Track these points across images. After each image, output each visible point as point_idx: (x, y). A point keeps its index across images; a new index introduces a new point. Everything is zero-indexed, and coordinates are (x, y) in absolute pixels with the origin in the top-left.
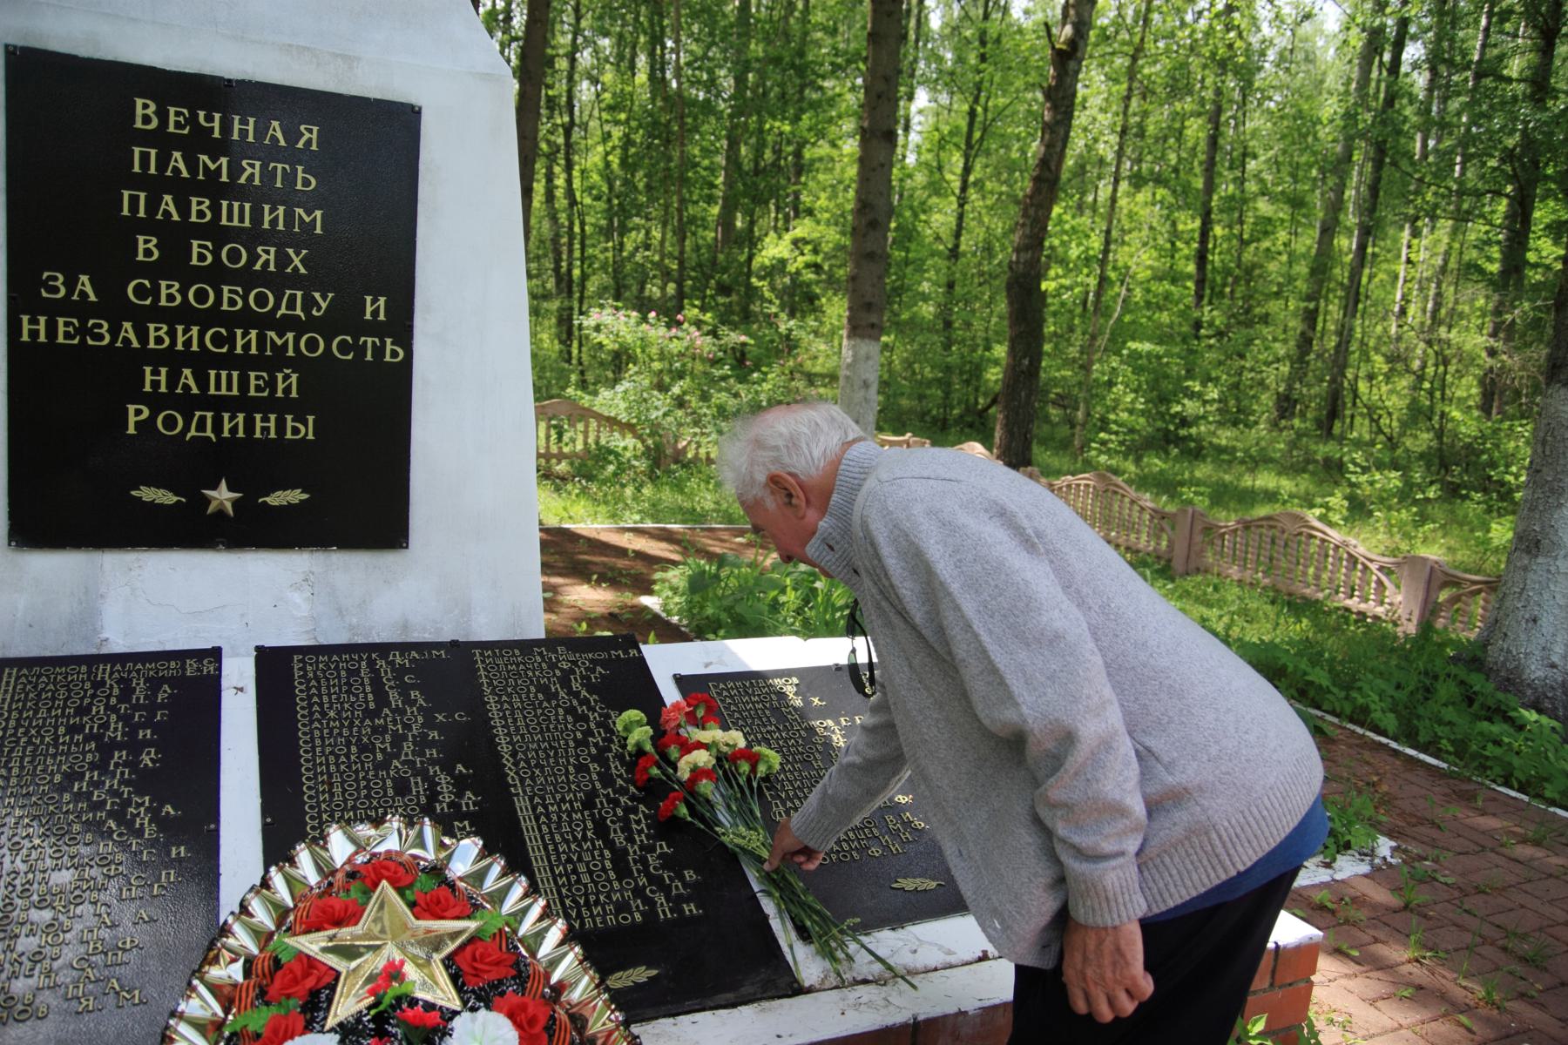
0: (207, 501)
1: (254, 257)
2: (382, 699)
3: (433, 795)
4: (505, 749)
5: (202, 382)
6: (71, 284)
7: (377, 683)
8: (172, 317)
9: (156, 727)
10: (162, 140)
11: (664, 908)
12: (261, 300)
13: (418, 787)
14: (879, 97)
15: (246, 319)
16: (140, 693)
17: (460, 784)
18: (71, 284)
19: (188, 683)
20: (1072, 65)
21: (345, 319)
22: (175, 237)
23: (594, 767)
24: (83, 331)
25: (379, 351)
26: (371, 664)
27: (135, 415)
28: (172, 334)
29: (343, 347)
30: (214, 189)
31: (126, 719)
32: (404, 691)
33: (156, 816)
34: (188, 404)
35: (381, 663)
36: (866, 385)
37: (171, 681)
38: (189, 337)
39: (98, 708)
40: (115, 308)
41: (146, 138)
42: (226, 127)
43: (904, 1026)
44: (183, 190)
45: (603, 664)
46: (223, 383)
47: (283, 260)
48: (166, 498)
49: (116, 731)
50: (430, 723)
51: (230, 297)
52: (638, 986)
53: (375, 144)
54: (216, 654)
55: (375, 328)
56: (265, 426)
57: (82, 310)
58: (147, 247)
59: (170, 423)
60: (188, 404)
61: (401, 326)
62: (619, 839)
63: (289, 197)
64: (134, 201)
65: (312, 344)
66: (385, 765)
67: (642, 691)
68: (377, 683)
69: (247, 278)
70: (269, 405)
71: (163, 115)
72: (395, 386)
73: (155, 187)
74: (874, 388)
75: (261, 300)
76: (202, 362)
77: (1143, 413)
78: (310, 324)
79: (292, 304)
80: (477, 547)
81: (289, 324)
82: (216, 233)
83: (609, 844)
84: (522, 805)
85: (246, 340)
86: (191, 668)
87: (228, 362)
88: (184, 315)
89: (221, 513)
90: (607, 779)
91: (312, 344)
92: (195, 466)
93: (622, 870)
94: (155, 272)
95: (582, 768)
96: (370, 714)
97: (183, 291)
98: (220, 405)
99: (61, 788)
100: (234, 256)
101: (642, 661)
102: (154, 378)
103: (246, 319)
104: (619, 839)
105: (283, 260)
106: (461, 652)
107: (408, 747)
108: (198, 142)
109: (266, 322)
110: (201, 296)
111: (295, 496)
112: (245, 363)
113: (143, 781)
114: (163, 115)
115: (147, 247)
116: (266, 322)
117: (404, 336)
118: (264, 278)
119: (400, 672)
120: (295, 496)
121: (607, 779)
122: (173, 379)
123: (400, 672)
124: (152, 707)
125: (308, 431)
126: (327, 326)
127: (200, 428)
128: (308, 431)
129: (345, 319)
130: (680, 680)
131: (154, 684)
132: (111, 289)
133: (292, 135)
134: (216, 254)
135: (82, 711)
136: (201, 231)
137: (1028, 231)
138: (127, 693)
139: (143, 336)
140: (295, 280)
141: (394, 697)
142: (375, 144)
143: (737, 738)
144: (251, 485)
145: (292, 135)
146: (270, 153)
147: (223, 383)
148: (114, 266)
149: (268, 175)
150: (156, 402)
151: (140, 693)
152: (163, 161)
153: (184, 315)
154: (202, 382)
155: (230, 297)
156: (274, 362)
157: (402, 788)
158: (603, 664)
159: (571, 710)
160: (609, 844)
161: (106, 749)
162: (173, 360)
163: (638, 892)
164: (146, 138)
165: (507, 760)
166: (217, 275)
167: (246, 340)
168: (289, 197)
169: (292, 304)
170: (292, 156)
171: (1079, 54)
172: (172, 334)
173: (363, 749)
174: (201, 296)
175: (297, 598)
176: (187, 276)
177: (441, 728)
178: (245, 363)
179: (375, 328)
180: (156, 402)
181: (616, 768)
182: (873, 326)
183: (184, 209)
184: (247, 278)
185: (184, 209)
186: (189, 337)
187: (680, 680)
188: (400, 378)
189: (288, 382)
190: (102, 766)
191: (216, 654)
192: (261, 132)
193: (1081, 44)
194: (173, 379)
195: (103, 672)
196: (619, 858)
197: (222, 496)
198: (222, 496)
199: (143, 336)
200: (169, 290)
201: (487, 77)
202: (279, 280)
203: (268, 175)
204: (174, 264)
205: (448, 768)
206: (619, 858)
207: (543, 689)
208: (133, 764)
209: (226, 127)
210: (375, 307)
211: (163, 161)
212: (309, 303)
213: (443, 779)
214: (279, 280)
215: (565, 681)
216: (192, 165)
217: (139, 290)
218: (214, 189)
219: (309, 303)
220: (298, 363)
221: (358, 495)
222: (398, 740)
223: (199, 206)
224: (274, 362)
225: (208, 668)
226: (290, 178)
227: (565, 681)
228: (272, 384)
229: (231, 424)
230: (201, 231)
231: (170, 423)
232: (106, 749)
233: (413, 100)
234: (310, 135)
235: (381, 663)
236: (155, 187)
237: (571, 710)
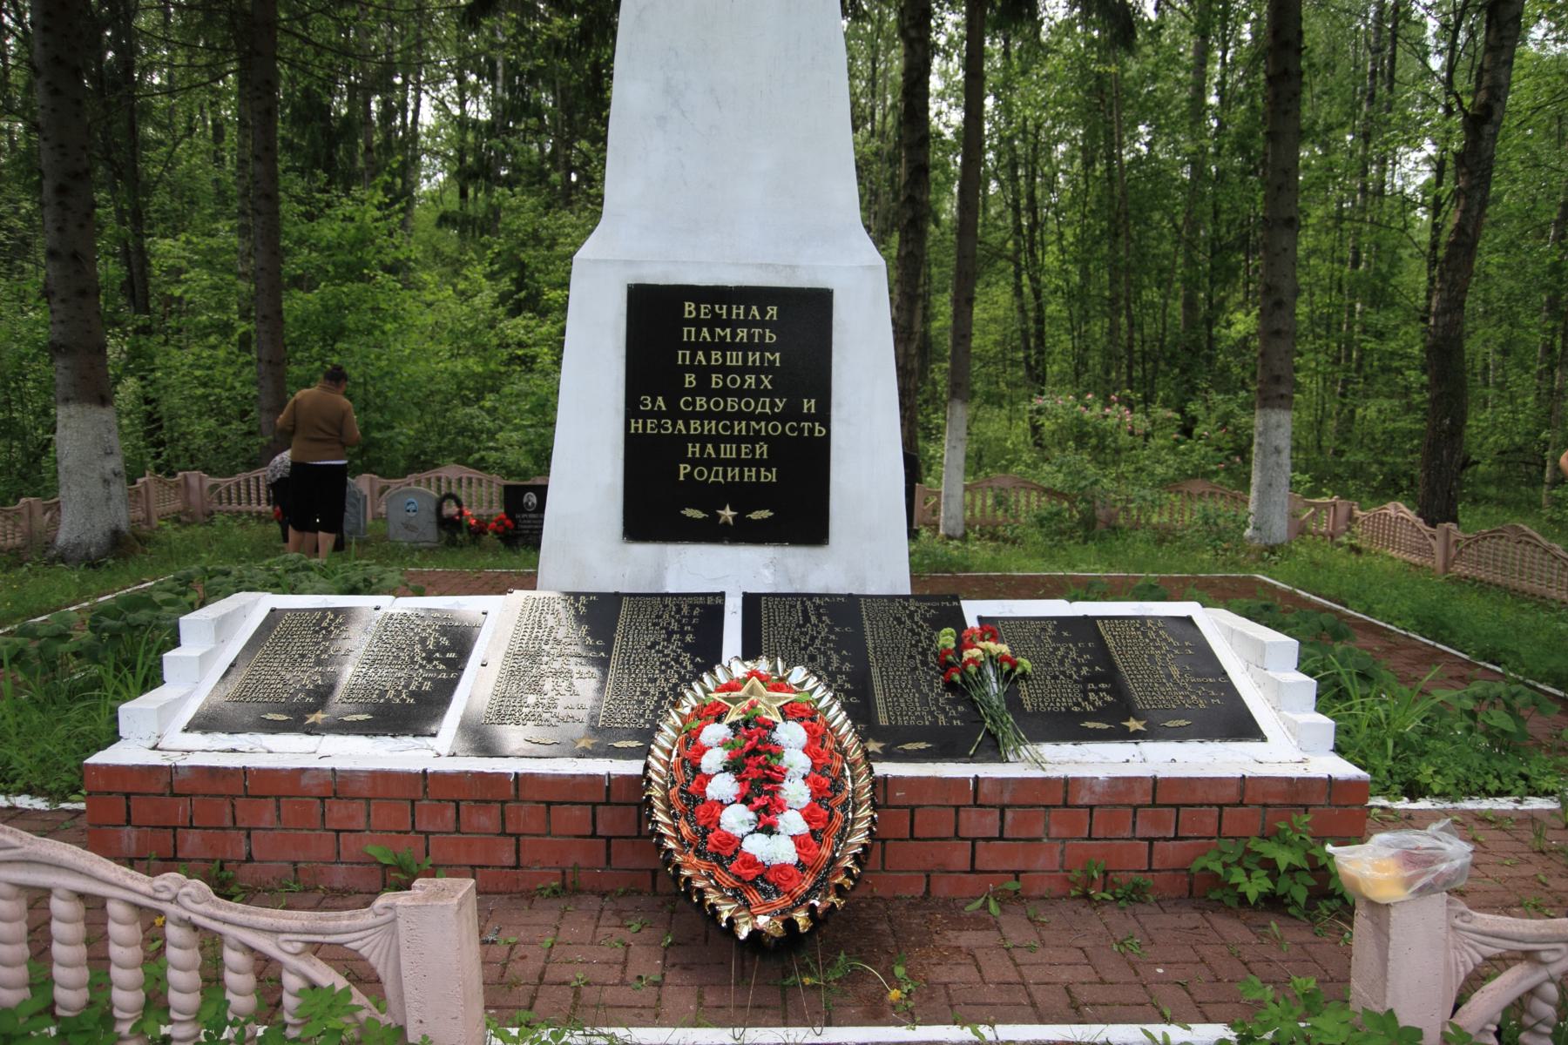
0: (719, 516)
1: (744, 381)
2: (807, 619)
3: (829, 663)
4: (870, 644)
5: (717, 451)
6: (654, 402)
7: (805, 611)
8: (701, 416)
9: (693, 626)
10: (697, 323)
11: (942, 720)
12: (748, 405)
13: (821, 659)
14: (1279, 188)
15: (740, 416)
16: (685, 611)
17: (843, 660)
18: (654, 402)
19: (708, 610)
20: (1488, 129)
21: (793, 413)
22: (704, 373)
23: (919, 657)
24: (659, 426)
25: (811, 430)
26: (803, 603)
27: (684, 469)
28: (702, 425)
29: (792, 429)
30: (723, 346)
31: (679, 621)
32: (819, 616)
33: (692, 662)
34: (709, 463)
35: (808, 603)
36: (1278, 451)
37: (701, 606)
38: (711, 427)
39: (666, 616)
40: (674, 413)
41: (690, 323)
42: (729, 312)
43: (1059, 779)
44: (707, 348)
45: (936, 608)
46: (728, 451)
47: (759, 382)
48: (697, 514)
49: (675, 626)
50: (831, 631)
51: (732, 404)
52: (919, 750)
53: (808, 311)
54: (722, 595)
55: (810, 417)
56: (750, 474)
57: (658, 415)
58: (690, 380)
59: (701, 474)
60: (709, 463)
61: (823, 415)
62: (926, 690)
63: (762, 347)
64: (684, 356)
65: (775, 428)
66: (805, 649)
67: (958, 620)
68: (805, 611)
69: (740, 393)
70: (751, 463)
71: (698, 309)
72: (822, 448)
73: (694, 347)
74: (1286, 453)
75: (748, 405)
76: (717, 440)
77: (255, 383)
78: (775, 417)
79: (764, 406)
80: (866, 546)
81: (763, 417)
82: (724, 370)
83: (920, 692)
84: (875, 671)
85: (740, 427)
86: (710, 601)
87: (731, 439)
88: (708, 415)
89: (726, 523)
90: (924, 663)
91: (775, 428)
92: (711, 497)
93: (924, 703)
94: (694, 393)
95: (911, 657)
96: (798, 625)
97: (708, 402)
98: (726, 463)
99: (650, 648)
100: (734, 381)
101: (960, 608)
102: (693, 450)
103: (740, 416)
104: (926, 690)
105: (759, 382)
106: (853, 600)
107: (818, 642)
108: (716, 321)
109: (750, 417)
110: (717, 404)
111: (766, 514)
112: (739, 440)
113: (687, 648)
114: (698, 309)
115: (690, 380)
116: (750, 417)
117: (826, 423)
118: (749, 393)
119: (818, 608)
120: (766, 514)
121: (924, 663)
122: (703, 450)
123: (818, 608)
124: (691, 617)
125: (772, 477)
126: (783, 418)
127: (716, 476)
128: (772, 477)
129: (793, 413)
130: (980, 619)
131: (692, 607)
132: (672, 402)
133: (763, 312)
134: (724, 381)
135: (658, 617)
136: (716, 369)
137: (1445, 295)
138: (679, 610)
139: (687, 427)
140: (766, 393)
141: (814, 619)
142: (808, 311)
143: (1004, 648)
144: (742, 508)
145: (763, 312)
146: (749, 323)
147: (728, 451)
148: (674, 391)
149: (751, 336)
150: (694, 462)
151: (685, 611)
152: (698, 333)
153: (708, 415)
154: (717, 451)
155: (732, 404)
156: (754, 439)
157: (812, 658)
158: (936, 608)
159: (912, 630)
160: (920, 692)
161: (670, 634)
162: (702, 439)
163: (931, 713)
164: (690, 323)
165: (871, 651)
166: (725, 392)
167: (740, 427)
168: (762, 347)
169: (764, 406)
170: (762, 324)
171: (1495, 118)
172: (702, 425)
173: (794, 641)
174: (717, 404)
175: (766, 572)
176: (710, 393)
177: (836, 634)
178: (739, 440)
179: (810, 417)
180: (694, 462)
181: (931, 658)
182: (1282, 396)
183: (708, 358)
184: (740, 393)
185: (708, 358)
186: (711, 427)
187: (980, 619)
188: (824, 445)
189: (762, 450)
190: (668, 640)
191: (722, 595)
192: (747, 312)
193: (1497, 106)
194: (703, 450)
195: (667, 601)
196: (924, 697)
197: (727, 514)
198: (727, 514)
199: (687, 427)
200: (701, 401)
201: (871, 268)
202: (757, 394)
203: (751, 336)
204: (703, 388)
205: (838, 652)
206: (924, 697)
207: (896, 619)
208: (682, 641)
209: (729, 312)
210: (809, 405)
211: (698, 333)
212: (773, 405)
213: (835, 657)
214: (757, 394)
215: (911, 616)
216: (712, 334)
217: (687, 404)
218: (723, 346)
219: (773, 405)
220: (767, 439)
221: (800, 513)
222: (813, 639)
223: (716, 355)
224: (754, 439)
225: (718, 601)
226: (762, 336)
227: (911, 616)
228: (753, 451)
229: (733, 473)
230: (716, 369)
231: (701, 474)
232: (670, 634)
233: (829, 286)
234: (772, 311)
235: (808, 603)
236: (694, 347)
237: (912, 630)
